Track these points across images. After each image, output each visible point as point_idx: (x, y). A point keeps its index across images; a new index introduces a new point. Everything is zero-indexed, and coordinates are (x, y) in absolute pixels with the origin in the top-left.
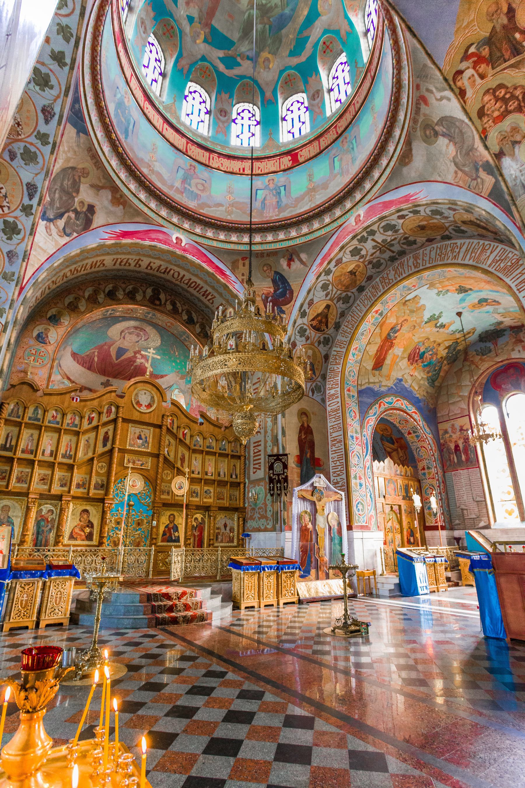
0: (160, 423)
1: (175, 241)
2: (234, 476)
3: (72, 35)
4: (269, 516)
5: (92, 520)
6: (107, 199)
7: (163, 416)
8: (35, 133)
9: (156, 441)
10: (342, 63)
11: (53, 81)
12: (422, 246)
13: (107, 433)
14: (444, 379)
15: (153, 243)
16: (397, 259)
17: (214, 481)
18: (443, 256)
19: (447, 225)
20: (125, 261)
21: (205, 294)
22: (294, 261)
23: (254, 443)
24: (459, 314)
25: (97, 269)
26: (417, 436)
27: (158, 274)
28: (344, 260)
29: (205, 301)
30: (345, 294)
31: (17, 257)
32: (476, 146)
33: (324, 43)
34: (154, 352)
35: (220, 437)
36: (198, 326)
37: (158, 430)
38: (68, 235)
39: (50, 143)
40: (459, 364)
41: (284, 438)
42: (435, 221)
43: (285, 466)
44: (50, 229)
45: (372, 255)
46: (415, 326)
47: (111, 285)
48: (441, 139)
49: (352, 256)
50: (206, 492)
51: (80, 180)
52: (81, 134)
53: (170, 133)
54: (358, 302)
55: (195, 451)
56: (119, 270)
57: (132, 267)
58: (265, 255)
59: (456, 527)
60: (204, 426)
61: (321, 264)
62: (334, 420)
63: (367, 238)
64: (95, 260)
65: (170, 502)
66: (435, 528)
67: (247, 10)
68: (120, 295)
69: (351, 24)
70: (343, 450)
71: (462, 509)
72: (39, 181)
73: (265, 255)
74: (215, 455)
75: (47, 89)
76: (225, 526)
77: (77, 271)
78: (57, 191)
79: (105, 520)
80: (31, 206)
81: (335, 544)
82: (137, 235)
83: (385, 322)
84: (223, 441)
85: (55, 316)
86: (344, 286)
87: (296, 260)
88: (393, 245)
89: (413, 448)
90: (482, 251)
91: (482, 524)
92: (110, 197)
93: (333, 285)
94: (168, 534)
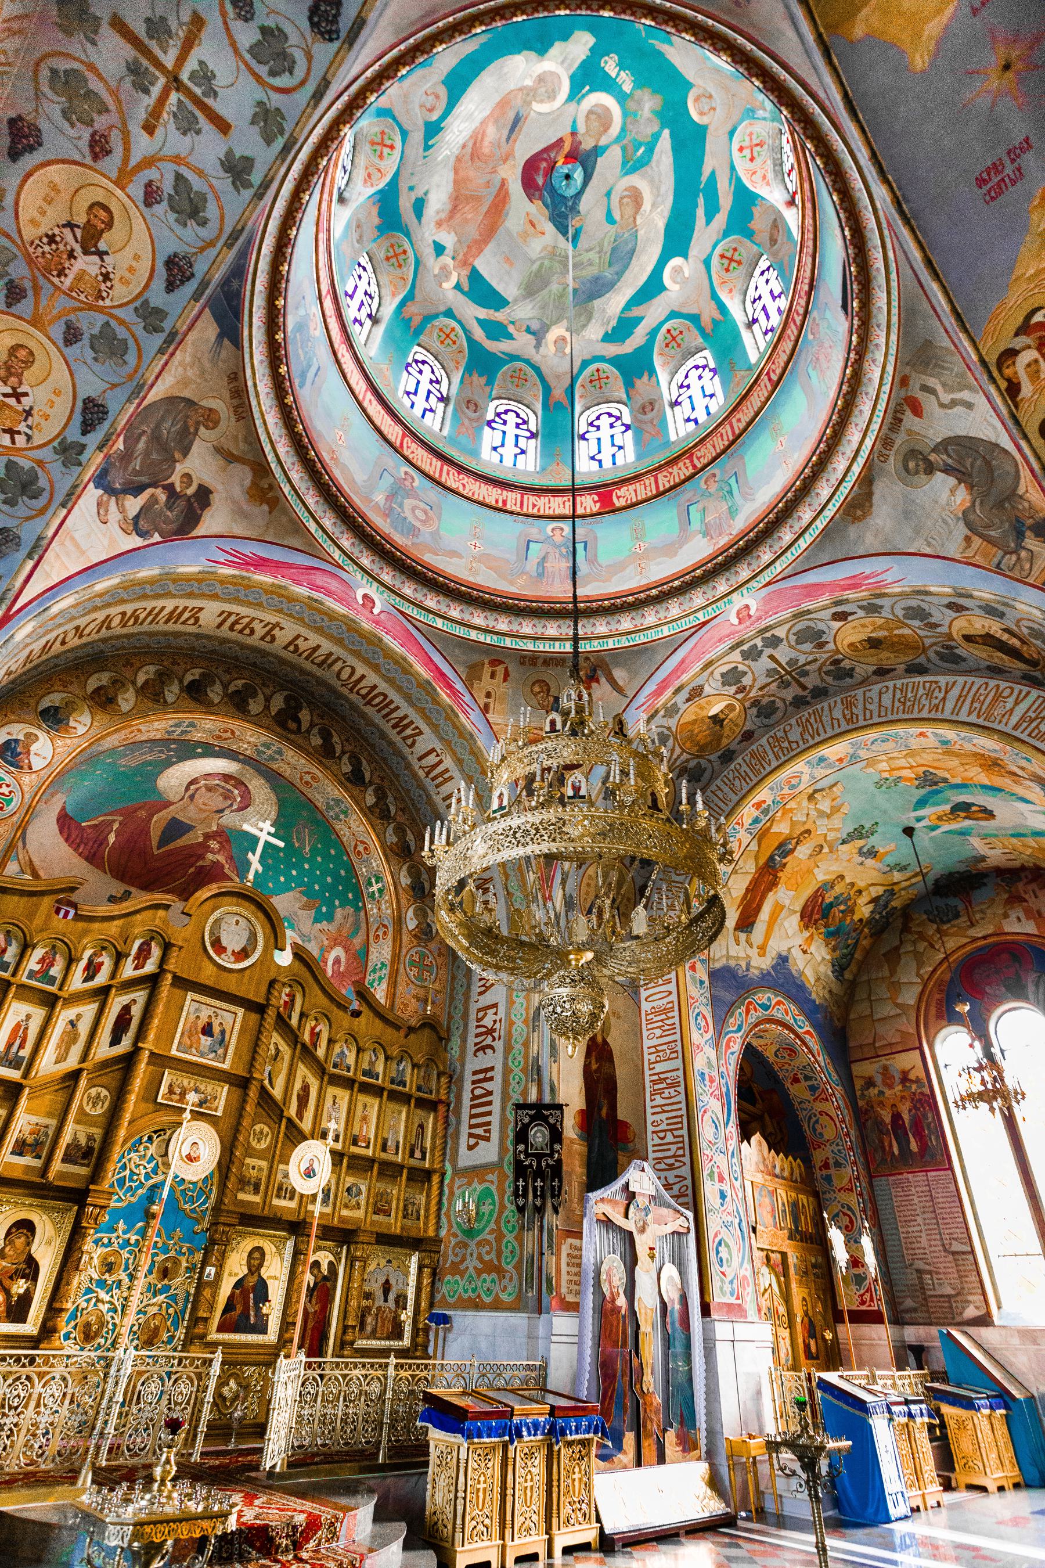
0: (261, 1000)
1: (361, 602)
2: (418, 1154)
3: (282, 132)
4: (509, 1267)
5: (37, 1256)
6: (242, 486)
7: (272, 983)
8: (138, 304)
9: (247, 1043)
10: (697, 367)
11: (211, 211)
12: (864, 682)
13: (126, 1009)
14: (862, 965)
15: (315, 595)
16: (808, 703)
17: (372, 1161)
18: (908, 704)
19: (928, 642)
20: (245, 621)
21: (401, 725)
22: (598, 681)
23: (475, 1073)
24: (909, 831)
25: (179, 627)
26: (813, 1089)
27: (307, 665)
28: (707, 690)
29: (396, 739)
30: (695, 761)
31: (18, 545)
32: (1021, 491)
33: (669, 331)
34: (273, 830)
35: (395, 1052)
36: (371, 790)
37: (254, 1017)
38: (140, 534)
39: (163, 331)
40: (891, 940)
41: (555, 1066)
42: (906, 631)
43: (556, 1135)
44: (107, 511)
45: (761, 689)
46: (822, 847)
47: (200, 671)
48: (939, 476)
49: (724, 684)
50: (349, 1190)
51: (197, 430)
52: (226, 342)
53: (375, 409)
54: (718, 782)
55: (336, 1081)
56: (223, 641)
57: (253, 641)
58: (540, 661)
59: (907, 1316)
60: (362, 1019)
61: (659, 692)
62: (658, 1032)
63: (761, 651)
64: (181, 603)
65: (258, 1212)
66: (859, 1317)
67: (538, 259)
68: (215, 694)
69: (722, 308)
70: (683, 1106)
71: (918, 1271)
72: (114, 402)
73: (540, 661)
74: (381, 1097)
75: (191, 223)
76: (386, 1287)
77: (137, 619)
78: (144, 439)
79: (76, 1255)
80: (83, 447)
81: (675, 1355)
82: (287, 572)
83: (769, 828)
84: (401, 1061)
85: (57, 709)
86: (697, 744)
87: (603, 680)
88: (805, 674)
89: (802, 1115)
90: (995, 700)
91: (970, 1312)
92: (248, 483)
93: (676, 739)
94: (239, 1308)
